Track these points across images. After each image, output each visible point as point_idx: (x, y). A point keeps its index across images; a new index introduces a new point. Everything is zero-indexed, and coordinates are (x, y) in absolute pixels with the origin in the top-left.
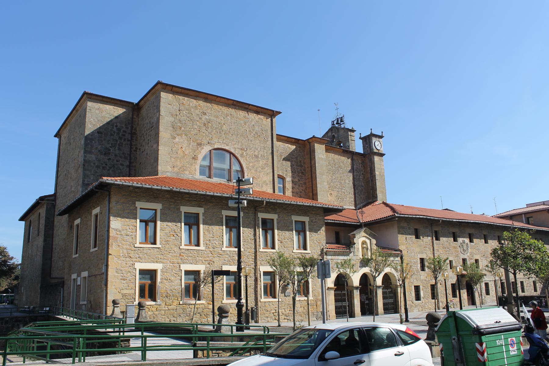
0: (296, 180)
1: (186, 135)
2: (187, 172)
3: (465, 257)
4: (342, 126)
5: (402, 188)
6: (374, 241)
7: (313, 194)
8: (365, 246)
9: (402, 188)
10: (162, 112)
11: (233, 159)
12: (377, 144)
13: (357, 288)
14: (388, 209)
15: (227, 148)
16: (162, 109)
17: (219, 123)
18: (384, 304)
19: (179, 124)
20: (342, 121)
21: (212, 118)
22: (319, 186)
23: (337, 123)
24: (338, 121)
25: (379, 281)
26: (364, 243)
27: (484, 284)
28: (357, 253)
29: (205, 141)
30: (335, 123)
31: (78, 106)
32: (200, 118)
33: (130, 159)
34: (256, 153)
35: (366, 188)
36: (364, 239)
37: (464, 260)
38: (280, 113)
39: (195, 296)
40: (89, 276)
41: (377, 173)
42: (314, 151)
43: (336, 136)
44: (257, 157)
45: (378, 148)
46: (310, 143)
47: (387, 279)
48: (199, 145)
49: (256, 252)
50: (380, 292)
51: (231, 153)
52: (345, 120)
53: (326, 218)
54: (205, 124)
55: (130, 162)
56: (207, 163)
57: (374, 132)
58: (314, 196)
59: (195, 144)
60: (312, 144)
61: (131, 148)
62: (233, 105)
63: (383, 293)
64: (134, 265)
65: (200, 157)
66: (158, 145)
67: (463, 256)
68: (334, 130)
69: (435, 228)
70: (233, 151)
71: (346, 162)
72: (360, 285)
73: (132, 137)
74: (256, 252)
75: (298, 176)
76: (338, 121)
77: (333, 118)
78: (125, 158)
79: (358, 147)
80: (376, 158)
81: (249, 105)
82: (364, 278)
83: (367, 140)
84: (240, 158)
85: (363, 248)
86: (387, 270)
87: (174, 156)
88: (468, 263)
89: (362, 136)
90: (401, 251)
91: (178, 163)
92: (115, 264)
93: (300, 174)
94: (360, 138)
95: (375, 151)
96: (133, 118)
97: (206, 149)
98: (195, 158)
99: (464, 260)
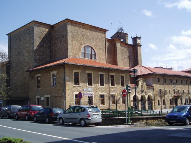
0: (109, 56)
1: (77, 41)
2: (77, 56)
3: (175, 89)
4: (122, 32)
5: (151, 60)
6: (145, 83)
7: (115, 63)
8: (142, 85)
9: (151, 60)
10: (69, 31)
11: (93, 50)
12: (138, 41)
13: (140, 101)
14: (150, 71)
15: (90, 45)
16: (68, 30)
17: (88, 35)
18: (148, 107)
19: (74, 36)
20: (122, 29)
21: (85, 33)
22: (118, 59)
23: (120, 30)
24: (120, 29)
25: (147, 98)
26: (142, 84)
27: (157, 101)
28: (139, 89)
29: (83, 43)
30: (119, 29)
31: (27, 25)
32: (81, 34)
33: (51, 49)
34: (100, 47)
35: (135, 59)
36: (142, 82)
37: (174, 90)
38: (108, 30)
39: (78, 104)
40: (50, 97)
41: (138, 53)
42: (116, 45)
43: (120, 36)
44: (100, 49)
45: (139, 43)
46: (114, 41)
47: (149, 97)
48: (81, 44)
49: (109, 87)
50: (147, 102)
51: (92, 48)
52: (124, 29)
53: (130, 74)
54: (83, 36)
55: (51, 50)
56: (83, 52)
57: (138, 36)
58: (115, 63)
59: (80, 44)
60: (115, 42)
61: (51, 44)
62: (92, 27)
63: (148, 102)
64: (73, 93)
65: (81, 49)
66: (67, 45)
67: (174, 89)
68: (118, 33)
69: (165, 78)
70: (92, 47)
71: (126, 49)
72: (133, 99)
73: (51, 39)
74: (109, 87)
75: (109, 55)
76: (120, 29)
77: (118, 27)
78: (49, 48)
79: (130, 42)
80: (138, 48)
81: (98, 27)
82: (142, 97)
83: (135, 39)
84: (95, 50)
85: (141, 85)
86: (149, 94)
87: (73, 49)
88: (176, 91)
89: (132, 37)
90: (153, 87)
91: (74, 52)
92: (68, 92)
93: (110, 54)
94: (132, 38)
95: (138, 44)
96: (51, 31)
97: (84, 46)
98: (80, 50)
99: (174, 90)
